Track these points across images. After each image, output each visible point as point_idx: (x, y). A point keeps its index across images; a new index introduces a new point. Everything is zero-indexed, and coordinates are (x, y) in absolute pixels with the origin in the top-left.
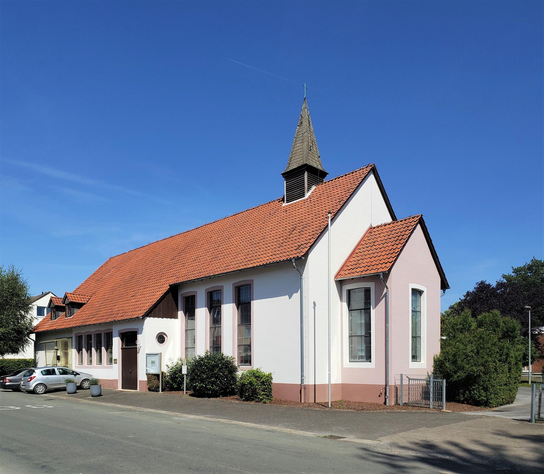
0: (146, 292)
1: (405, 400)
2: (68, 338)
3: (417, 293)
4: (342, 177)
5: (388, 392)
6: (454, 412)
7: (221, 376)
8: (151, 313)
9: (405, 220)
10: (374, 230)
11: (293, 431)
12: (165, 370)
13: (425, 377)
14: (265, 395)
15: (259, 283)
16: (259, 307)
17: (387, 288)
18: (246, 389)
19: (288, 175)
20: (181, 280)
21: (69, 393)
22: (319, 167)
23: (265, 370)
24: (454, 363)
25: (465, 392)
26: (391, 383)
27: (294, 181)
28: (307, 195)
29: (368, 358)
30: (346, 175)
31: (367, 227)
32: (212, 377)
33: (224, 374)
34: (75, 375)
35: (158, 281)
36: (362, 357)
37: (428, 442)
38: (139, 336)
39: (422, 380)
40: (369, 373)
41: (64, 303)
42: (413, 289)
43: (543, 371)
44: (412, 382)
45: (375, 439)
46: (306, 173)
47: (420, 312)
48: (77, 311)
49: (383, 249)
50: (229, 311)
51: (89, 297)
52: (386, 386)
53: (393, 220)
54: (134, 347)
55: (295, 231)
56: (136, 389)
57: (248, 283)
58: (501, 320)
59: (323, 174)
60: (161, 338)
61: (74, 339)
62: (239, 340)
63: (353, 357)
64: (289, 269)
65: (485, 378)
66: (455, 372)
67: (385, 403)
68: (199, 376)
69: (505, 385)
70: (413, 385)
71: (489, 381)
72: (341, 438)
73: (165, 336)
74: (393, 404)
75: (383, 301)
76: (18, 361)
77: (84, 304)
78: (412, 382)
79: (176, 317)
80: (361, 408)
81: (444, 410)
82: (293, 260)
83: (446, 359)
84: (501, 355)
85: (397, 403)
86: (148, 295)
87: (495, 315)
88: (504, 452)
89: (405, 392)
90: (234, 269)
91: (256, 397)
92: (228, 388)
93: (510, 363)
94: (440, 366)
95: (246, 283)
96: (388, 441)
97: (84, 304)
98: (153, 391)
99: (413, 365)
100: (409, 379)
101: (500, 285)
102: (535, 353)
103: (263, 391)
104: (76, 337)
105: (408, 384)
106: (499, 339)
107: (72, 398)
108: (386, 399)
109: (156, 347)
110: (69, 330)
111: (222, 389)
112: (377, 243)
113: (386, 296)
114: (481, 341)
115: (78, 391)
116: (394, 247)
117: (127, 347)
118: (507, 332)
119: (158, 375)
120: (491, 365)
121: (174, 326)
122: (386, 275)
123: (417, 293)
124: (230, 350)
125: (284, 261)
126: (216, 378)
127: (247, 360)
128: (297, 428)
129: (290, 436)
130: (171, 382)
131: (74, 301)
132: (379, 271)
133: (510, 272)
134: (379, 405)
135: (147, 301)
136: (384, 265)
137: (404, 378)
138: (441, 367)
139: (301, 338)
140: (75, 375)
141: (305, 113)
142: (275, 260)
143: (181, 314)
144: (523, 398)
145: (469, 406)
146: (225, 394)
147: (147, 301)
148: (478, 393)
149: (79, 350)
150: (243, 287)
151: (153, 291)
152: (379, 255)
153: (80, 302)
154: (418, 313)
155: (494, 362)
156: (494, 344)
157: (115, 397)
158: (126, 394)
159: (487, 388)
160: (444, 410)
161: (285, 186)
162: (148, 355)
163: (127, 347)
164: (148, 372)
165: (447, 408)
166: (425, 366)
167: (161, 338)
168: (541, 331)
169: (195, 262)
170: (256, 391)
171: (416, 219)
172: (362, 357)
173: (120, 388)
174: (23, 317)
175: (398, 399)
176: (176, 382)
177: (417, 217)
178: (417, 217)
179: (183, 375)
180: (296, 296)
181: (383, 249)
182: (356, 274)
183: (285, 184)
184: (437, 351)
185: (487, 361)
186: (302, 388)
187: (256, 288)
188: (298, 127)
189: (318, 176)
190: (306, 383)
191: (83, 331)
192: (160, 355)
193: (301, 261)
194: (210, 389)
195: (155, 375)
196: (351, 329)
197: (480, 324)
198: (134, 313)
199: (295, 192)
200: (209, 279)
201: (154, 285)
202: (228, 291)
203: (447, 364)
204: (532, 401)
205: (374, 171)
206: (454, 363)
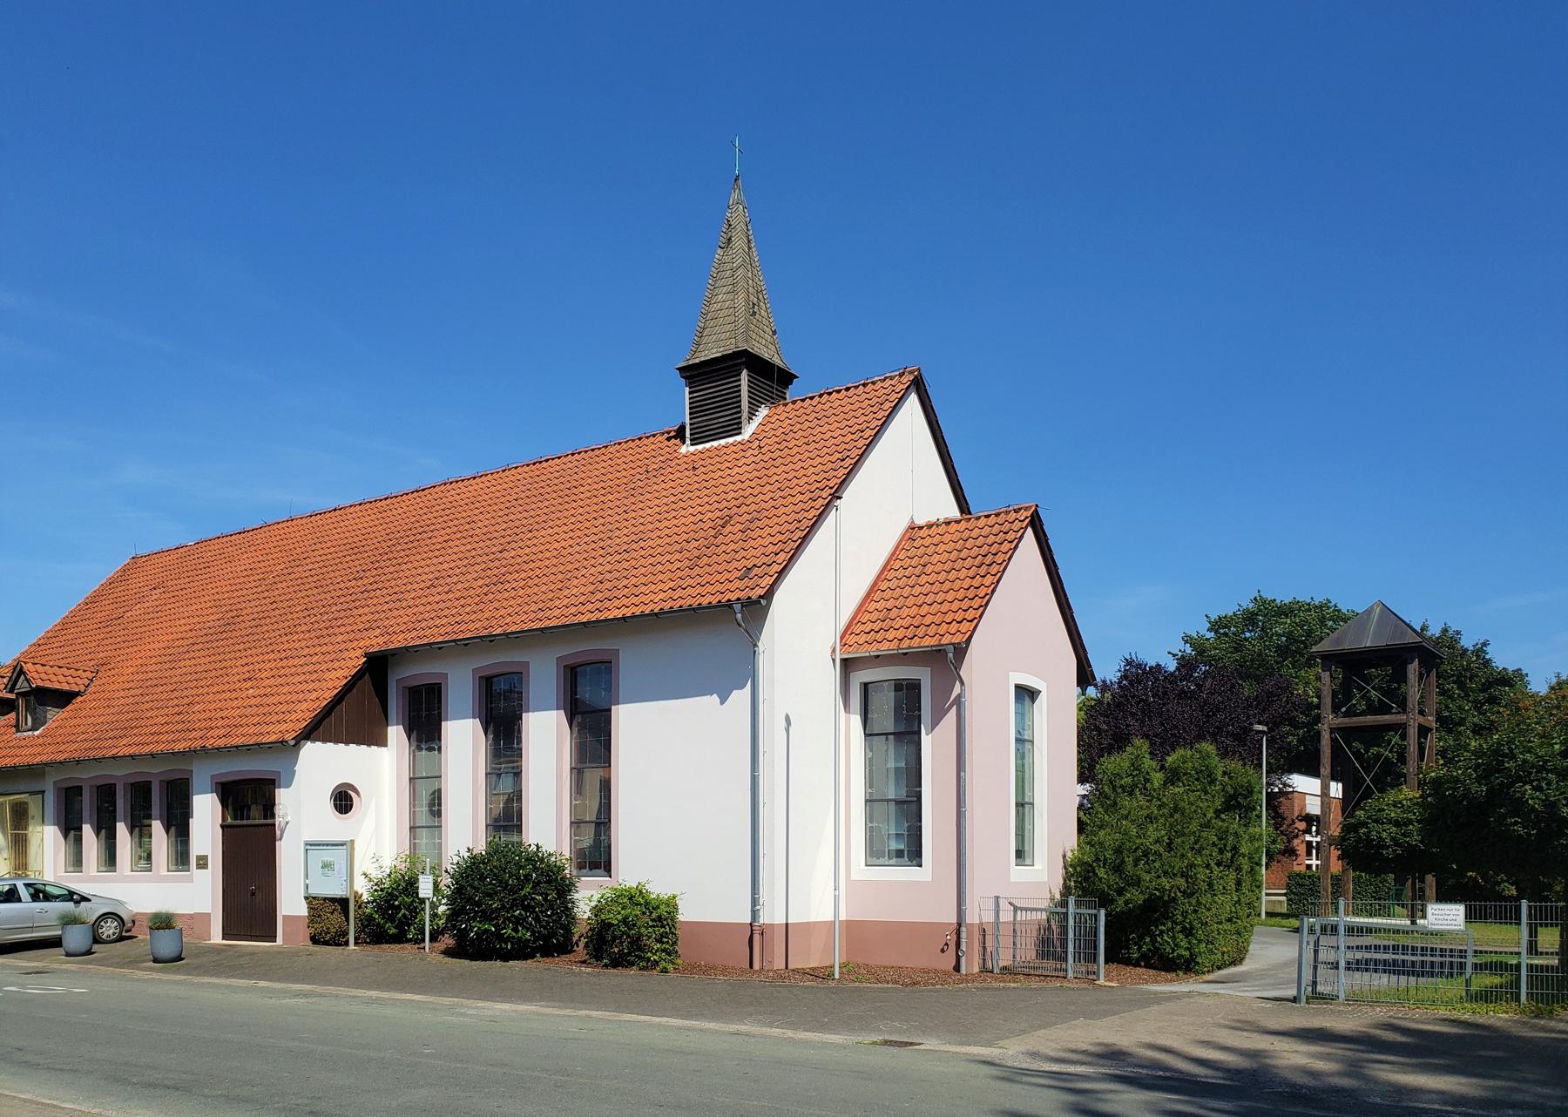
0: (287, 671)
1: (1005, 959)
2: (32, 793)
3: (1026, 694)
4: (838, 391)
5: (963, 941)
6: (1122, 986)
7: (539, 904)
8: (313, 731)
9: (997, 515)
10: (923, 533)
11: (790, 1033)
12: (363, 888)
13: (1045, 904)
14: (663, 950)
16: (635, 724)
17: (962, 683)
18: (614, 938)
19: (695, 374)
20: (398, 642)
21: (68, 955)
22: (777, 361)
23: (658, 889)
24: (1118, 869)
25: (1141, 938)
26: (972, 918)
27: (711, 389)
28: (749, 430)
29: (913, 853)
30: (848, 389)
31: (904, 525)
32: (514, 906)
33: (545, 899)
34: (77, 902)
35: (322, 641)
36: (899, 854)
37: (1106, 1045)
38: (282, 796)
39: (1036, 910)
40: (915, 894)
41: (11, 691)
42: (1017, 687)
43: (1288, 887)
44: (1021, 916)
45: (990, 1044)
46: (744, 374)
47: (1032, 742)
48: (55, 716)
49: (947, 585)
50: (546, 734)
51: (90, 675)
52: (959, 925)
53: (962, 512)
55: (728, 528)
56: (273, 938)
57: (606, 658)
58: (1219, 766)
59: (786, 378)
60: (343, 800)
61: (50, 798)
62: (574, 809)
63: (875, 853)
64: (718, 631)
65: (1185, 905)
66: (1120, 892)
67: (957, 968)
68: (479, 904)
69: (1229, 920)
70: (1026, 923)
71: (1195, 911)
72: (911, 1044)
74: (976, 970)
75: (952, 715)
77: (78, 694)
78: (1021, 916)
79: (381, 741)
80: (911, 980)
81: (1101, 981)
82: (737, 607)
83: (1098, 859)
84: (1221, 851)
85: (985, 970)
86: (298, 679)
87: (1205, 756)
88: (1268, 1061)
89: (1006, 941)
90: (564, 621)
91: (639, 957)
92: (554, 934)
93: (1239, 869)
94: (1082, 879)
95: (600, 658)
96: (1023, 1049)
97: (78, 694)
98: (326, 943)
99: (1019, 874)
100: (1016, 909)
101: (1185, 664)
102: (1274, 842)
103: (659, 941)
104: (58, 790)
105: (992, 920)
106: (1218, 813)
107: (72, 965)
108: (958, 958)
109: (332, 825)
110: (34, 772)
111: (542, 937)
112: (929, 569)
113: (958, 701)
114: (1177, 816)
115: (96, 947)
116: (976, 583)
117: (239, 822)
118: (1234, 797)
119: (343, 903)
120: (1202, 874)
121: (381, 767)
122: (961, 651)
123: (1026, 694)
124: (547, 828)
125: (710, 606)
126: (526, 908)
127: (597, 858)
128: (794, 1026)
129: (806, 1043)
130: (389, 917)
131: (47, 685)
132: (945, 641)
133: (1201, 629)
134: (945, 973)
135: (301, 696)
136: (954, 627)
137: (1004, 904)
138: (1086, 879)
139: (739, 802)
140: (77, 902)
141: (738, 216)
142: (686, 603)
143: (395, 733)
144: (1272, 952)
145: (1152, 972)
146: (547, 951)
147: (301, 696)
148: (1170, 940)
149: (70, 828)
150: (588, 668)
151: (311, 668)
152: (940, 598)
153: (66, 687)
154: (1028, 745)
155: (1208, 866)
156: (1207, 825)
157: (217, 963)
158: (241, 954)
159: (1192, 928)
160: (1101, 981)
161: (687, 401)
162: (311, 845)
163: (239, 822)
164: (313, 891)
165: (1108, 977)
166: (1039, 879)
167: (343, 800)
168: (1285, 785)
169: (433, 590)
170: (637, 940)
171: (1023, 514)
172: (899, 854)
173: (216, 937)
175: (988, 957)
176: (392, 919)
177: (1026, 509)
178: (1026, 509)
179: (422, 901)
180: (741, 697)
181: (947, 585)
182: (885, 645)
183: (687, 396)
184: (1070, 840)
185: (1192, 866)
186: (754, 934)
188: (720, 251)
189: (773, 380)
190: (764, 919)
191: (84, 775)
192: (348, 846)
193: (756, 609)
194: (509, 939)
195: (333, 900)
196: (870, 781)
197: (1173, 776)
198: (265, 728)
199: (713, 416)
200: (489, 642)
201: (312, 651)
202: (543, 675)
203: (1101, 873)
204: (1300, 955)
205: (918, 385)
206: (1118, 869)
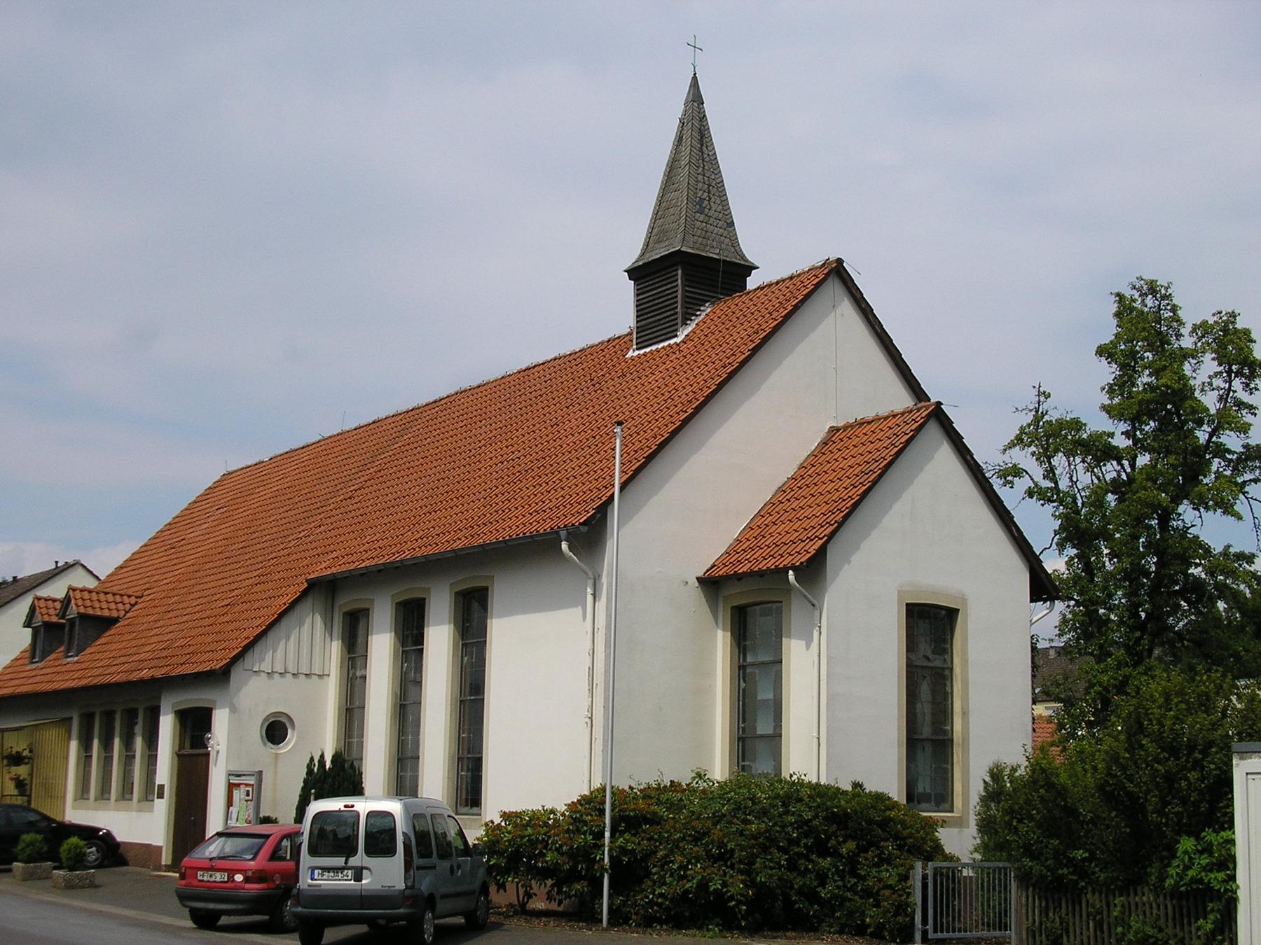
15: (503, 589)
16: (506, 634)
41: (63, 618)
51: (133, 600)
54: (202, 751)
73: (288, 725)
76: (945, 693)
77: (114, 621)
97: (114, 621)
109: (259, 753)
153: (106, 613)
174: (563, 814)
187: (497, 599)
